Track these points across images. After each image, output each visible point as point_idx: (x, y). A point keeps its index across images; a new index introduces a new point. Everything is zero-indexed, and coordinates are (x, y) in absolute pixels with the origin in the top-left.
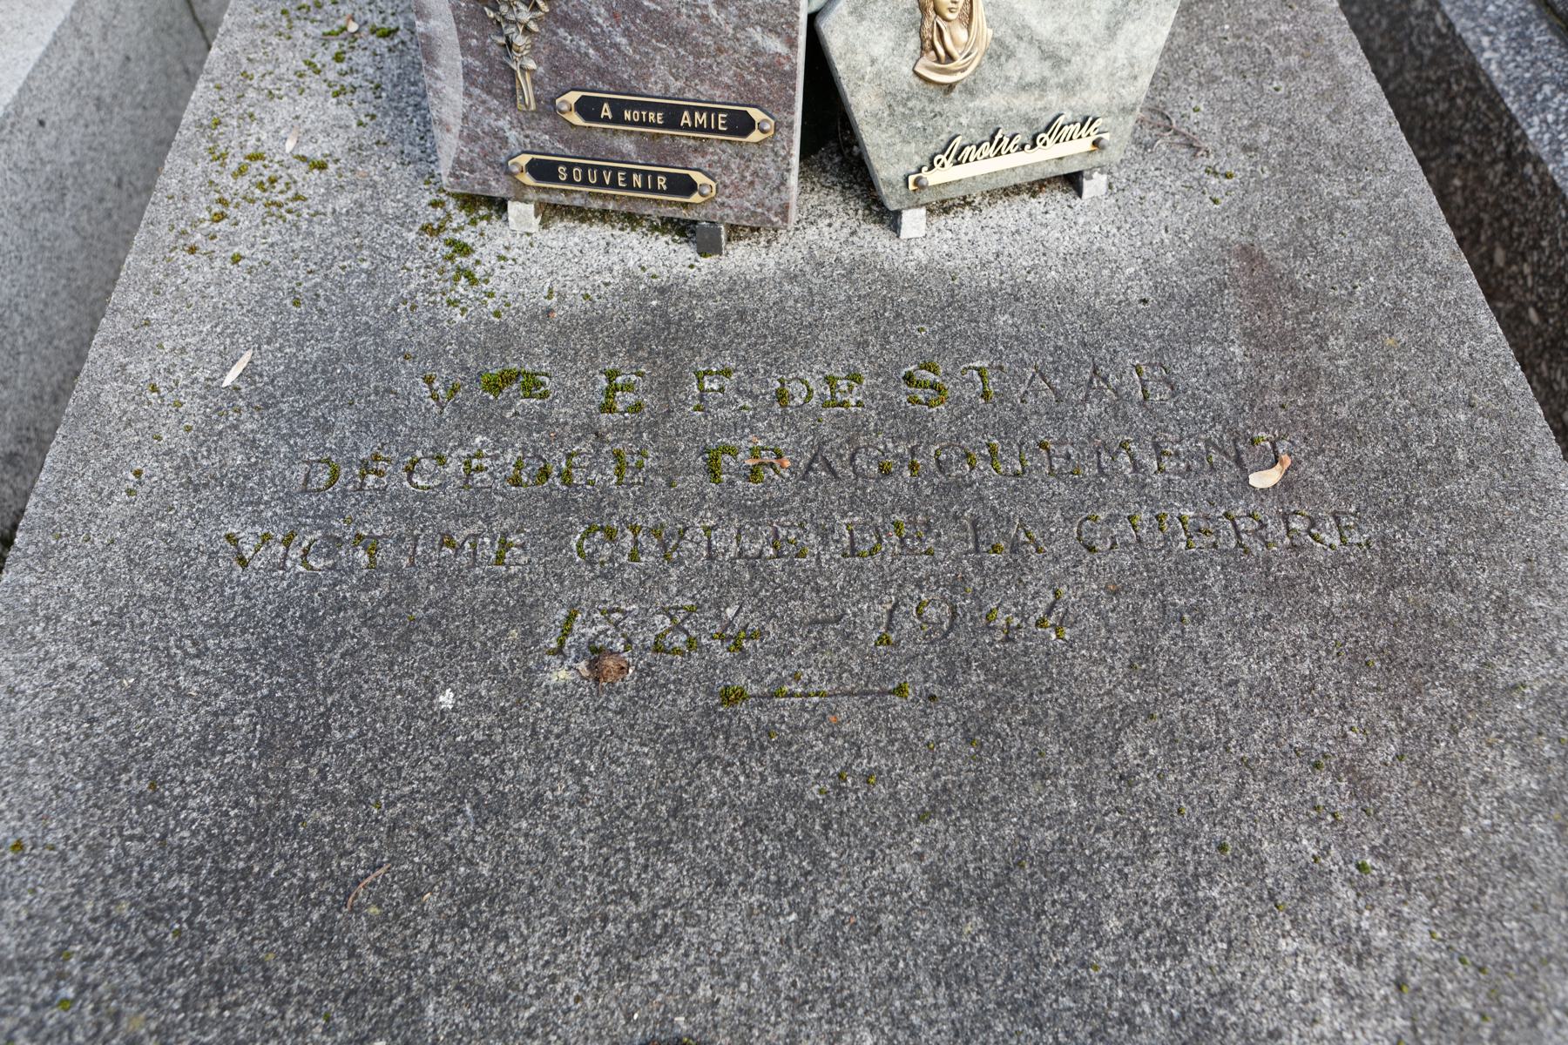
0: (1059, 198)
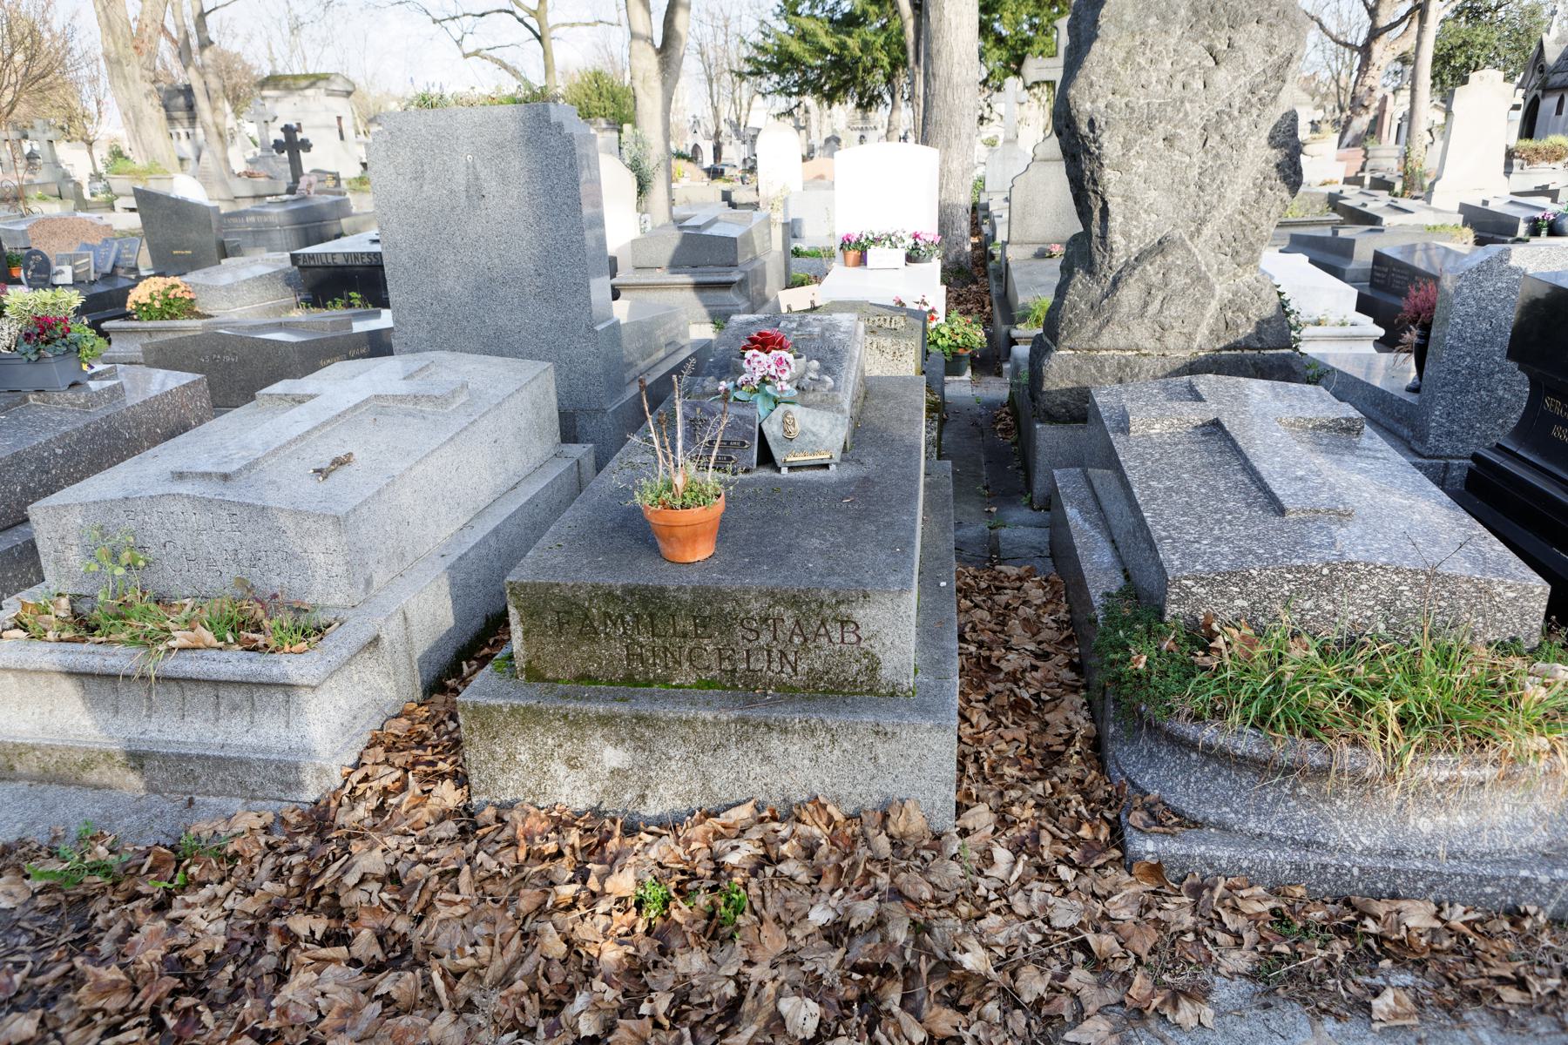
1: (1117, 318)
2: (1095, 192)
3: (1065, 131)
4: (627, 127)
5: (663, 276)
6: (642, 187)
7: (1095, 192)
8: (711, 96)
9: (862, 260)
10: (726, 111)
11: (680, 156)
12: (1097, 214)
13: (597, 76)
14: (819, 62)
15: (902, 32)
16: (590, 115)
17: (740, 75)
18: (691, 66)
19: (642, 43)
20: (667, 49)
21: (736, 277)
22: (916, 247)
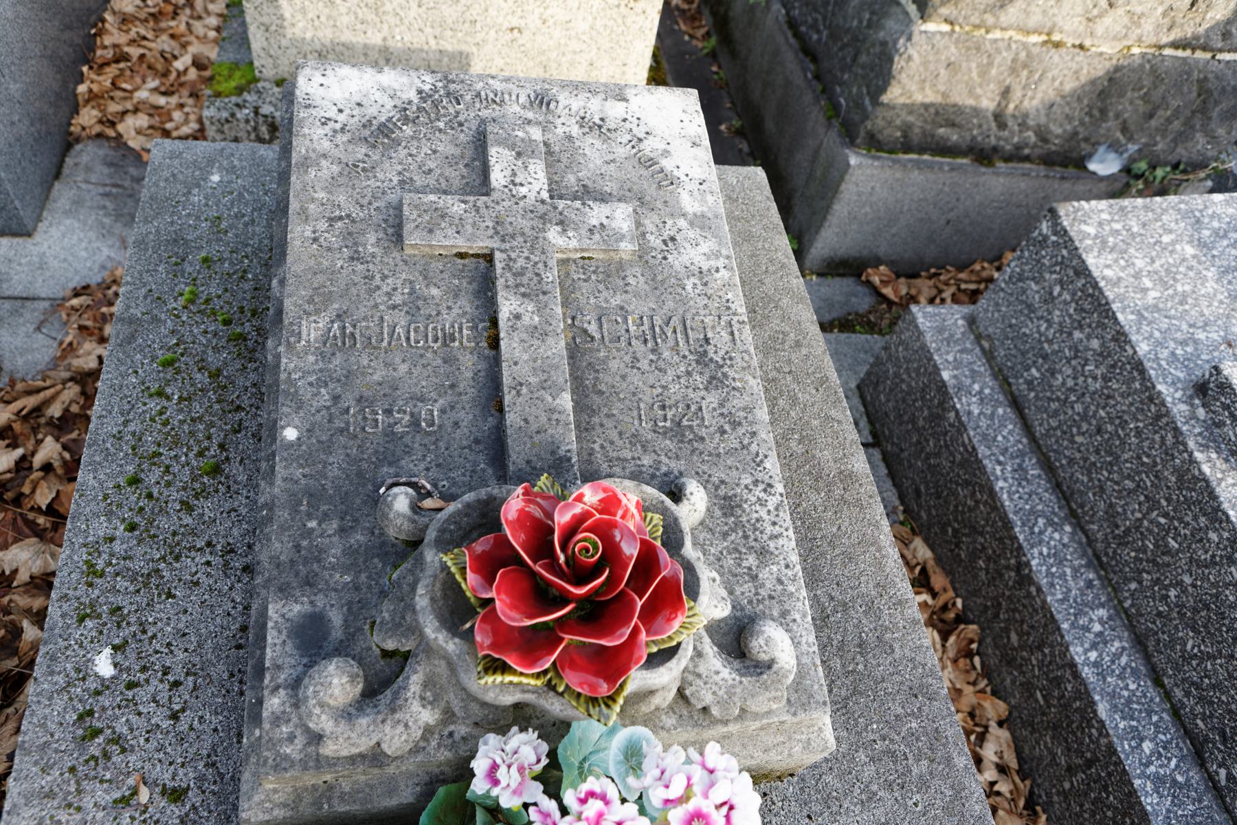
0: (733, 813)
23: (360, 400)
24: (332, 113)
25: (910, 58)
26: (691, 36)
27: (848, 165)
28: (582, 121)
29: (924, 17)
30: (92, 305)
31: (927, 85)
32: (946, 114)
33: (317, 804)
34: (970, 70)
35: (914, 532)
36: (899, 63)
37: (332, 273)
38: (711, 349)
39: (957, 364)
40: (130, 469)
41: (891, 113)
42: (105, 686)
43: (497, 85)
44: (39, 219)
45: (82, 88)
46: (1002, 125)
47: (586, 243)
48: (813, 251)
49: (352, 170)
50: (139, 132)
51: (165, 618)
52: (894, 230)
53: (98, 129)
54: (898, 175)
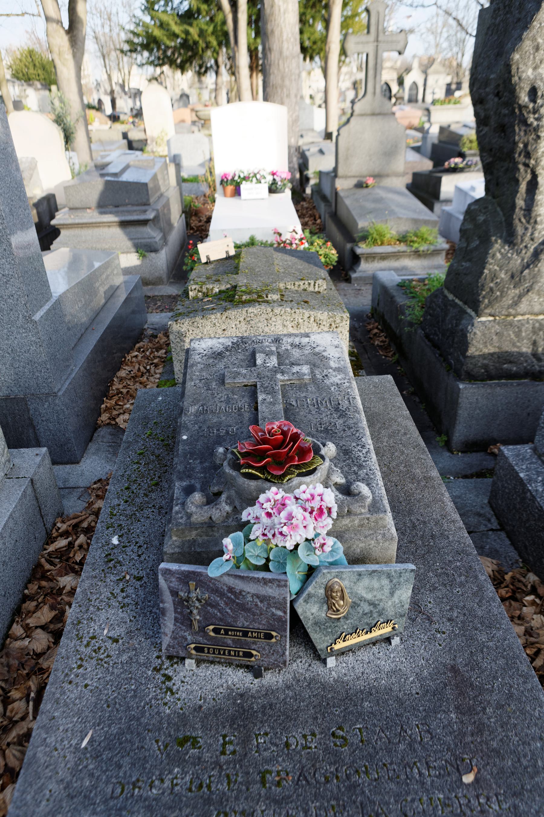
1: (536, 287)
2: (526, 165)
3: (492, 101)
4: (54, 88)
5: (92, 216)
6: (68, 138)
7: (526, 165)
8: (105, 67)
9: (237, 192)
10: (116, 77)
11: (90, 107)
12: (523, 187)
13: (31, 53)
14: (173, 44)
15: (224, 23)
16: (29, 79)
17: (122, 51)
18: (90, 46)
19: (54, 25)
20: (74, 29)
21: (151, 215)
22: (274, 182)
23: (208, 427)
24: (202, 351)
25: (475, 334)
26: (386, 356)
27: (459, 389)
28: (292, 345)
29: (479, 315)
30: (100, 488)
31: (488, 345)
32: (504, 357)
33: (190, 547)
34: (509, 335)
35: (529, 571)
36: (470, 336)
37: (201, 394)
38: (341, 407)
39: (528, 469)
40: (126, 485)
41: (473, 361)
42: (115, 547)
43: (260, 338)
44: (85, 449)
45: (103, 406)
46: (539, 360)
47: (291, 377)
48: (454, 438)
49: (208, 366)
50: (125, 421)
51: (137, 528)
52: (498, 422)
53: (108, 421)
54: (489, 391)
